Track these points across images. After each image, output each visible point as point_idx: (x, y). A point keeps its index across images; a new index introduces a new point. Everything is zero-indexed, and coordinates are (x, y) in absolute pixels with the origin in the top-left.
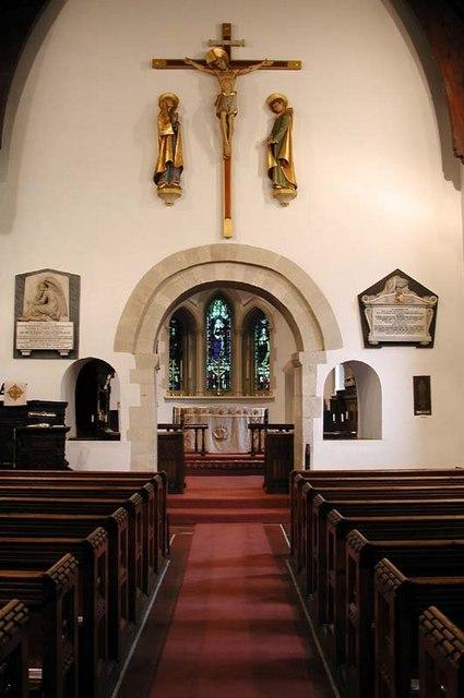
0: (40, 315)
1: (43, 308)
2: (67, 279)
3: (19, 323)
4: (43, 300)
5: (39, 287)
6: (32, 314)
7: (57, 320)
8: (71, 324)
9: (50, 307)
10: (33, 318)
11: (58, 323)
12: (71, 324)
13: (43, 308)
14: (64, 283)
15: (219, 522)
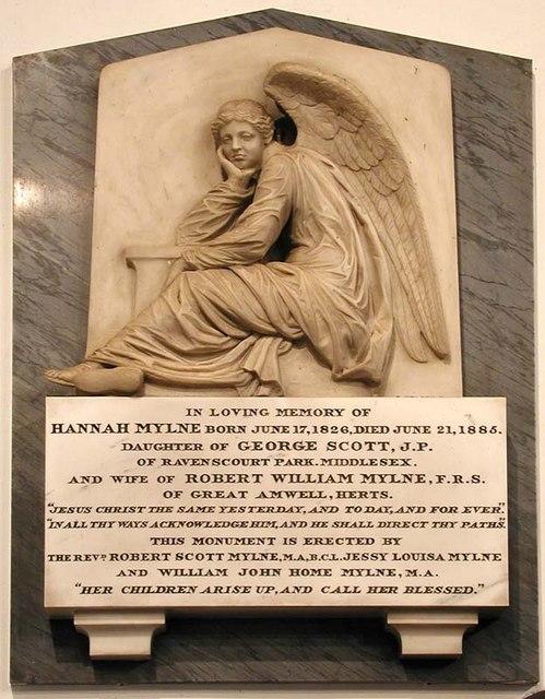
0: (225, 345)
1: (258, 289)
2: (435, 80)
3: (59, 410)
4: (260, 223)
5: (218, 135)
6: (170, 339)
7: (370, 383)
8: (492, 410)
9: (318, 281)
10: (176, 368)
11: (383, 409)
12: (492, 410)
13: (258, 289)
14: (415, 112)
15: (388, 49)
